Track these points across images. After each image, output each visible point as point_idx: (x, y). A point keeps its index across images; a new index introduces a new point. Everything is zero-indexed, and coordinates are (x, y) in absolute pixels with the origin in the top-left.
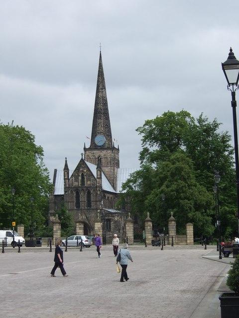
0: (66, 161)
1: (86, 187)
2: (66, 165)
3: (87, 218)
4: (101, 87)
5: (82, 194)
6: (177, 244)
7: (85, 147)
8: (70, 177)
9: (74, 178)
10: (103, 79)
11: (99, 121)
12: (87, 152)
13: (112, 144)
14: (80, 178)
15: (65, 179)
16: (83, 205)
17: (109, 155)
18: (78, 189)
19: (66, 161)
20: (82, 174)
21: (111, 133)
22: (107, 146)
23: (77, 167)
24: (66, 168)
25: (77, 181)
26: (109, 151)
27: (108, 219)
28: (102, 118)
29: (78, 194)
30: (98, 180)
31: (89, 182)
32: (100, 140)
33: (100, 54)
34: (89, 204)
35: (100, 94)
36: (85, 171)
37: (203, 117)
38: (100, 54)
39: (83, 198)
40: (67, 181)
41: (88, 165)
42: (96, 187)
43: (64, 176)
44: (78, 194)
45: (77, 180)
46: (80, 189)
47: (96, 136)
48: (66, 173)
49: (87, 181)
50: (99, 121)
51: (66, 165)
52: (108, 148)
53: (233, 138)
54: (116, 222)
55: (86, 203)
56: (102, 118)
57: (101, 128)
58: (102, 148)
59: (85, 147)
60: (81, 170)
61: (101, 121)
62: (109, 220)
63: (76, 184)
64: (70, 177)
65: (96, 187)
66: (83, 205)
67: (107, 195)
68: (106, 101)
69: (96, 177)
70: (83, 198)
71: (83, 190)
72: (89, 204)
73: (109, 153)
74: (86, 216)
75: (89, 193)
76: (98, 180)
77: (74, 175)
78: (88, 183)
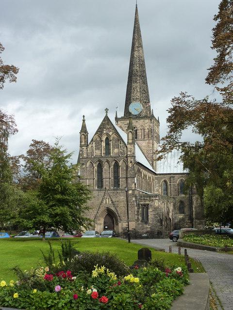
2: (84, 130)
3: (113, 202)
5: (105, 167)
7: (116, 116)
9: (94, 145)
10: (140, 36)
12: (119, 122)
14: (103, 144)
20: (107, 139)
22: (144, 114)
23: (100, 128)
24: (84, 130)
26: (147, 121)
27: (144, 205)
28: (138, 81)
29: (100, 166)
31: (116, 150)
33: (136, 7)
34: (117, 183)
35: (136, 54)
36: (111, 133)
37: (47, 255)
38: (136, 7)
40: (85, 148)
41: (121, 136)
43: (81, 142)
44: (100, 166)
45: (98, 147)
46: (104, 160)
47: (130, 103)
49: (114, 148)
50: (134, 85)
52: (146, 117)
54: (156, 209)
55: (112, 182)
57: (137, 94)
58: (138, 117)
59: (116, 116)
60: (105, 132)
61: (137, 86)
62: (146, 207)
63: (97, 153)
67: (144, 172)
68: (143, 61)
69: (126, 142)
72: (117, 183)
73: (147, 124)
74: (112, 200)
75: (117, 166)
76: (129, 146)
77: (94, 139)
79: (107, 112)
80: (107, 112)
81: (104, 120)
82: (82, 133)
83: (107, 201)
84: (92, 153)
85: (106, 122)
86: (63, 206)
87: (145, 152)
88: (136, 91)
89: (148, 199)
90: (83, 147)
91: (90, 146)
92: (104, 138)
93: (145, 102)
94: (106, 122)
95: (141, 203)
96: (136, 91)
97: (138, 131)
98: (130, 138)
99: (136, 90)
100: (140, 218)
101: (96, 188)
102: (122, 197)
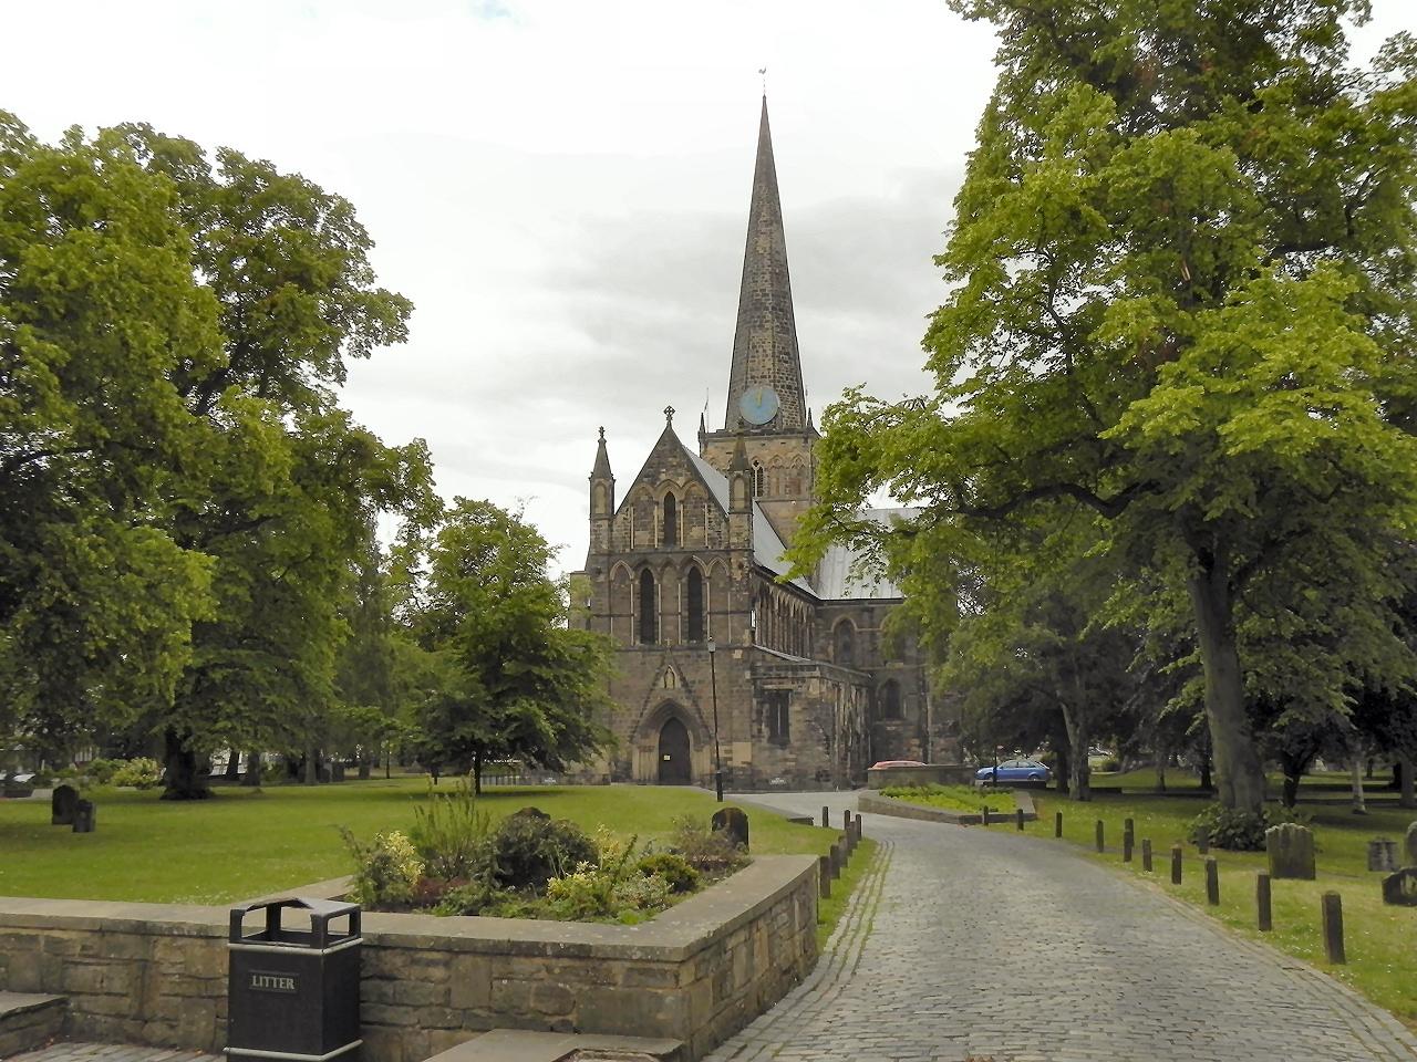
0: (602, 443)
1: (682, 551)
2: (603, 461)
3: (685, 684)
4: (765, 216)
6: (325, 201)
8: (617, 504)
10: (780, 275)
11: (757, 336)
13: (802, 420)
14: (658, 513)
15: (594, 518)
16: (671, 623)
17: (791, 455)
18: (645, 562)
19: (602, 443)
21: (799, 380)
23: (648, 464)
25: (644, 527)
26: (794, 443)
28: (767, 325)
30: (733, 519)
31: (696, 532)
32: (763, 405)
34: (695, 628)
39: (671, 598)
42: (728, 551)
44: (646, 579)
45: (642, 522)
48: (601, 490)
49: (689, 524)
51: (603, 461)
52: (790, 431)
53: (500, 788)
54: (811, 704)
56: (767, 325)
58: (766, 431)
62: (780, 699)
63: (642, 537)
64: (617, 504)
65: (728, 551)
66: (671, 623)
69: (725, 504)
70: (671, 598)
71: (668, 563)
72: (695, 628)
74: (683, 679)
76: (733, 519)
78: (692, 535)
79: (669, 418)
80: (669, 418)
90: (599, 523)
91: (620, 517)
93: (789, 387)
95: (770, 687)
97: (765, 474)
99: (761, 350)
100: (765, 730)
101: (638, 643)
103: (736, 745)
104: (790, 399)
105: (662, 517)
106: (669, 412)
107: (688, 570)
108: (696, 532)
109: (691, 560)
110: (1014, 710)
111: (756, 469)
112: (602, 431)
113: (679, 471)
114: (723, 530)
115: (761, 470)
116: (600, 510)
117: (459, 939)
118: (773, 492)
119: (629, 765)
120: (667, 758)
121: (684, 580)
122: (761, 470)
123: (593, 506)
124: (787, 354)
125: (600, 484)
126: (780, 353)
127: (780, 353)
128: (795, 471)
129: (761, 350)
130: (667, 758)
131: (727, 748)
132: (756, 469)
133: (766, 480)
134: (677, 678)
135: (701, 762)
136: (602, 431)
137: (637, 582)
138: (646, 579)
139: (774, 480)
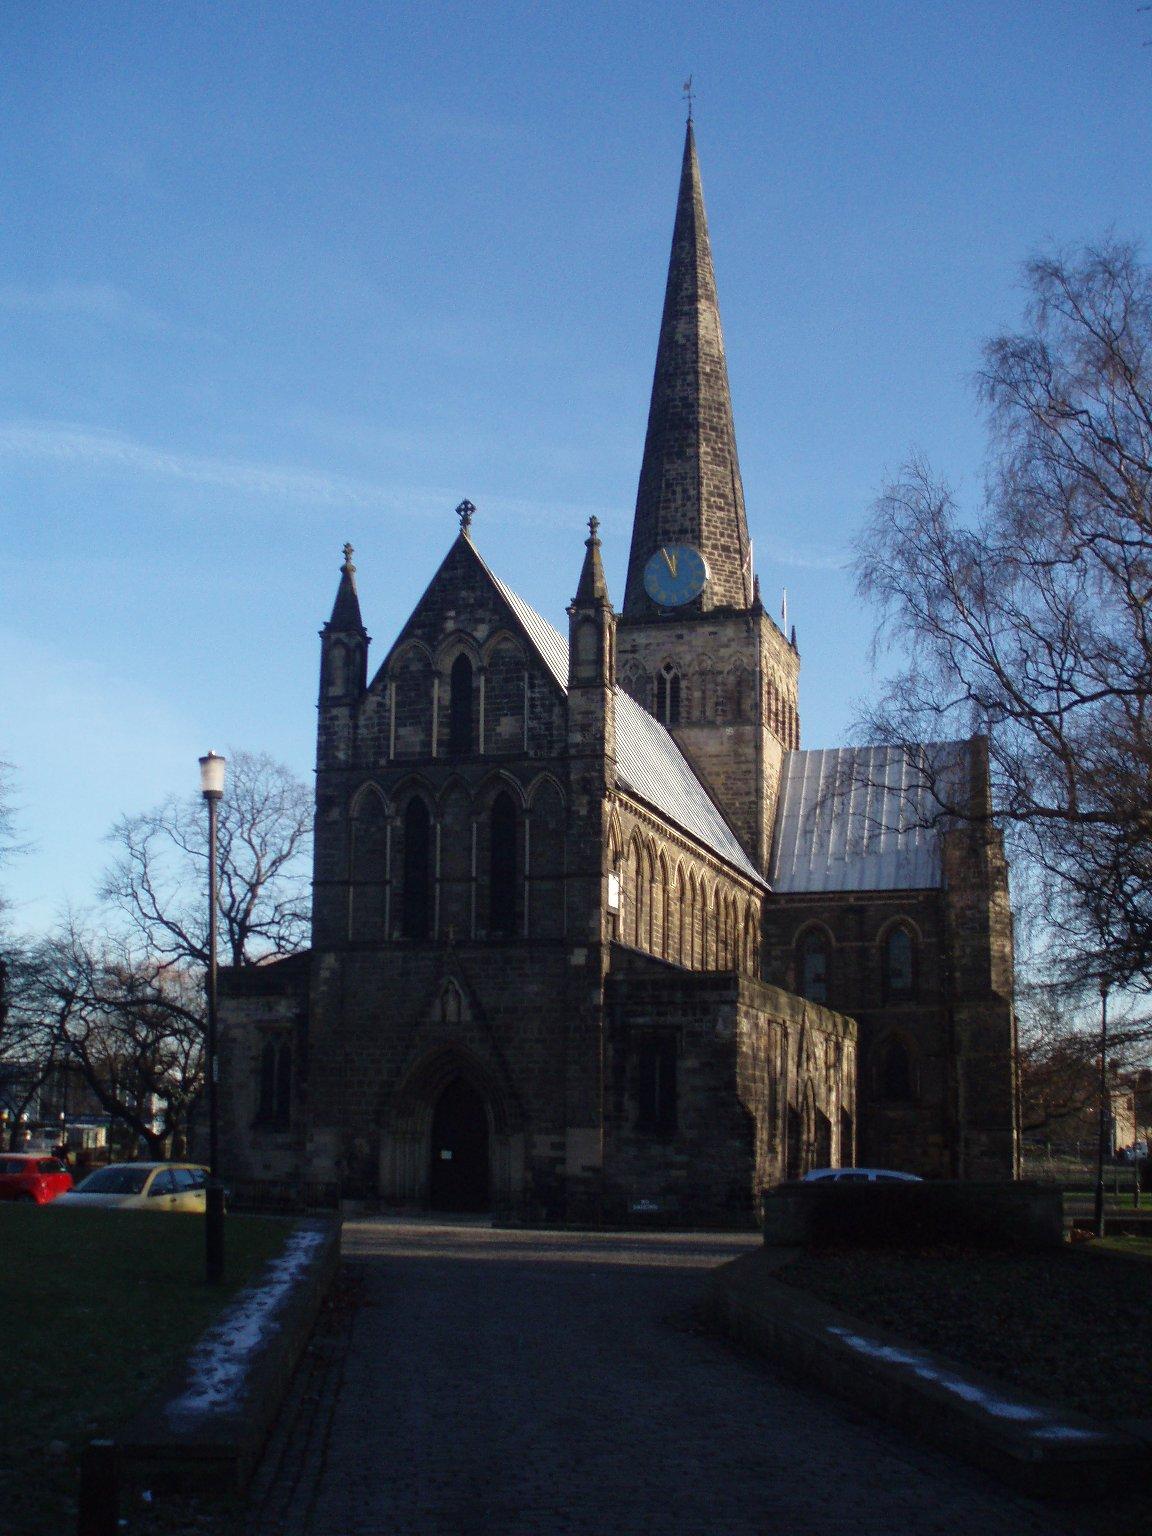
2: (347, 605)
14: (440, 692)
31: (506, 726)
33: (689, 130)
38: (689, 130)
44: (417, 818)
45: (414, 709)
48: (338, 653)
51: (347, 605)
60: (450, 625)
74: (475, 1004)
79: (465, 522)
80: (465, 522)
81: (450, 563)
82: (334, 636)
83: (452, 1006)
84: (380, 744)
85: (460, 572)
86: (303, 1269)
87: (718, 782)
88: (679, 496)
89: (679, 996)
90: (335, 712)
91: (372, 701)
92: (446, 664)
93: (726, 549)
94: (460, 572)
95: (641, 1020)
96: (679, 496)
97: (683, 684)
98: (583, 656)
99: (679, 489)
100: (630, 1107)
101: (396, 935)
102: (534, 988)
103: (576, 1136)
104: (727, 567)
105: (447, 697)
106: (466, 510)
107: (490, 798)
108: (506, 726)
109: (498, 778)
110: (281, 1524)
111: (668, 677)
112: (348, 551)
113: (480, 613)
114: (556, 720)
115: (676, 681)
116: (337, 690)
117: (691, 1269)
118: (696, 713)
119: (372, 1167)
120: (446, 1155)
121: (484, 817)
122: (676, 681)
123: (326, 681)
124: (722, 496)
125: (338, 642)
126: (711, 494)
127: (711, 494)
128: (732, 679)
129: (679, 489)
130: (446, 1155)
131: (555, 1138)
132: (668, 677)
133: (683, 694)
134: (465, 1001)
135: (510, 1165)
136: (348, 551)
137: (398, 822)
138: (417, 818)
139: (697, 694)
